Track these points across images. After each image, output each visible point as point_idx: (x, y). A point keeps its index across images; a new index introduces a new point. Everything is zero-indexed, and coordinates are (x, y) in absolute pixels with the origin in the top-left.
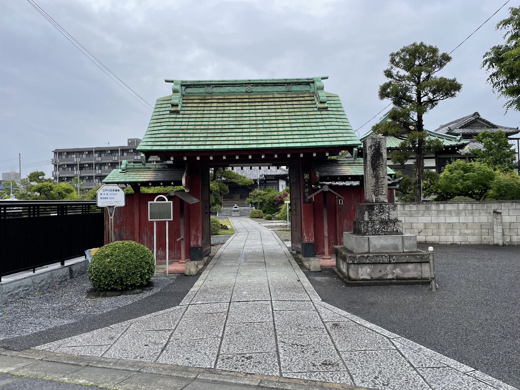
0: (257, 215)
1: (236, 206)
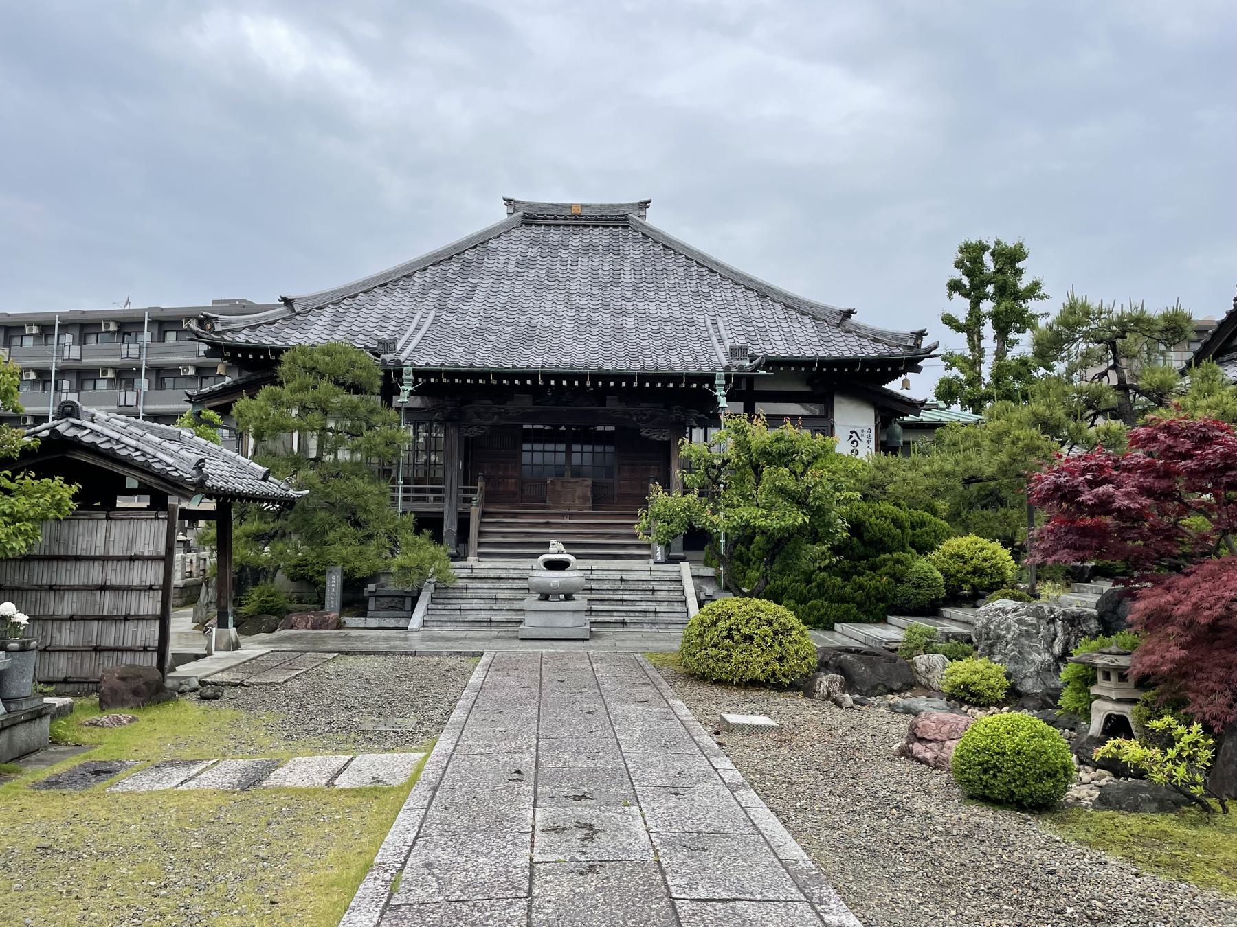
0: (756, 661)
1: (556, 551)
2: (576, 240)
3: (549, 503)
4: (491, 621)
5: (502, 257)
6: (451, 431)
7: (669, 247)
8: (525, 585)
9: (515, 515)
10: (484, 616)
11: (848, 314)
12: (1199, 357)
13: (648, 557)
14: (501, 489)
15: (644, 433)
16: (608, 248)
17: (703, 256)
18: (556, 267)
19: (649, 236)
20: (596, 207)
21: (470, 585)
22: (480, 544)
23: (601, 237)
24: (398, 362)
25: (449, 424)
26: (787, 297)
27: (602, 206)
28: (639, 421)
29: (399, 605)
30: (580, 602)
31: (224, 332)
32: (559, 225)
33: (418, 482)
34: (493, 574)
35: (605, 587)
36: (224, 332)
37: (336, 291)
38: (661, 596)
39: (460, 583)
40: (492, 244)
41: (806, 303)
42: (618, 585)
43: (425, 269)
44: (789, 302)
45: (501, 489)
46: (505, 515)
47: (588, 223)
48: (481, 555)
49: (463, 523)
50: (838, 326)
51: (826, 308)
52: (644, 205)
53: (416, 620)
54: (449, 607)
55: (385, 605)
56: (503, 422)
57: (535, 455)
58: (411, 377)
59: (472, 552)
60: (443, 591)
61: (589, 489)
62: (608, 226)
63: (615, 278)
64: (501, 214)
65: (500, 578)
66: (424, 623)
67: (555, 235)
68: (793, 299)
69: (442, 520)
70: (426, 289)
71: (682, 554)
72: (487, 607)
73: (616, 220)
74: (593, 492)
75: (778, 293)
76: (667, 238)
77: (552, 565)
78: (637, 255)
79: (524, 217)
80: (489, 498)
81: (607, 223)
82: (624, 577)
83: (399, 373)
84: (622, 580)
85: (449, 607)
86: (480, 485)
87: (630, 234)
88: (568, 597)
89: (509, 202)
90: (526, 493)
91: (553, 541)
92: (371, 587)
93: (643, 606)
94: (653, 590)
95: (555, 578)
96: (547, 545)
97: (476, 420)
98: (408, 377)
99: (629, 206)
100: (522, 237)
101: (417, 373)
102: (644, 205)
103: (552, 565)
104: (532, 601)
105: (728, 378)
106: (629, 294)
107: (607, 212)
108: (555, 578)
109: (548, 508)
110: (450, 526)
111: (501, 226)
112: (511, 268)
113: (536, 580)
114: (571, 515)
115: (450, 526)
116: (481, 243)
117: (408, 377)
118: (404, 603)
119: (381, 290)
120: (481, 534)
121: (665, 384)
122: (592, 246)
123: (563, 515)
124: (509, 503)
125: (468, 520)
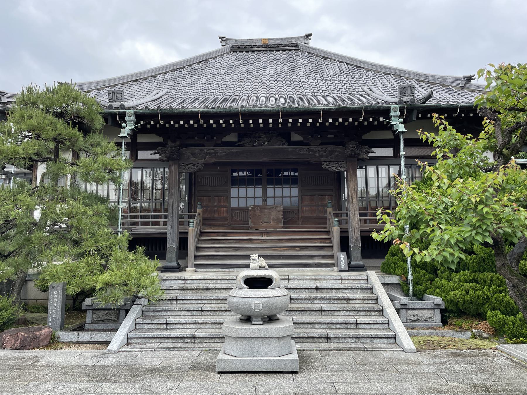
1: (257, 267)
2: (265, 57)
3: (251, 225)
4: (194, 338)
5: (217, 66)
6: (172, 168)
7: (326, 57)
8: (225, 306)
9: (225, 234)
10: (188, 331)
11: (470, 79)
12: (505, 168)
13: (333, 265)
14: (216, 215)
15: (325, 166)
16: (287, 60)
17: (350, 58)
18: (253, 69)
19: (312, 53)
20: (277, 39)
21: (180, 297)
22: (196, 257)
23: (282, 55)
24: (122, 106)
25: (170, 163)
26: (417, 74)
27: (281, 39)
28: (320, 156)
29: (113, 318)
30: (285, 325)
31: (9, 103)
32: (254, 51)
33: (155, 211)
34: (203, 285)
35: (303, 296)
36: (9, 103)
37: (100, 82)
38: (357, 305)
39: (173, 295)
40: (211, 61)
41: (432, 76)
42: (314, 294)
43: (166, 73)
44: (420, 78)
45: (216, 215)
46: (218, 234)
47: (272, 49)
48: (197, 266)
49: (183, 242)
50: (462, 88)
51: (451, 78)
52: (308, 36)
53: (117, 339)
54: (156, 321)
55: (102, 318)
56: (213, 160)
57: (243, 197)
58: (133, 118)
59: (189, 264)
60: (154, 307)
61: (281, 213)
62: (285, 50)
63: (292, 72)
64: (218, 46)
65: (208, 289)
66: (129, 341)
67: (251, 56)
68: (422, 75)
69: (165, 240)
70: (164, 82)
71: (361, 263)
72: (190, 319)
73: (290, 47)
74: (284, 216)
75: (410, 73)
76: (325, 52)
77: (254, 283)
78: (306, 62)
79: (233, 47)
80: (206, 222)
81: (285, 48)
82: (320, 286)
83: (123, 116)
84: (317, 289)
85: (156, 321)
86: (198, 211)
87: (300, 53)
88: (270, 319)
89: (223, 38)
90: (235, 218)
91: (254, 256)
92: (88, 301)
93: (341, 318)
94: (348, 299)
95: (257, 298)
96: (248, 257)
97: (192, 159)
98: (130, 118)
99: (298, 38)
100: (231, 59)
101: (139, 116)
102: (308, 36)
103: (254, 283)
104: (231, 325)
105: (401, 110)
106: (303, 79)
107: (284, 42)
108: (257, 298)
109: (250, 228)
110: (172, 244)
111: (217, 51)
112: (223, 71)
113: (235, 300)
114: (268, 233)
115: (172, 244)
116: (204, 60)
117: (130, 118)
118: (114, 316)
119: (134, 83)
120: (197, 249)
121: (345, 120)
122: (277, 60)
123: (262, 233)
124: (222, 225)
125: (187, 239)
